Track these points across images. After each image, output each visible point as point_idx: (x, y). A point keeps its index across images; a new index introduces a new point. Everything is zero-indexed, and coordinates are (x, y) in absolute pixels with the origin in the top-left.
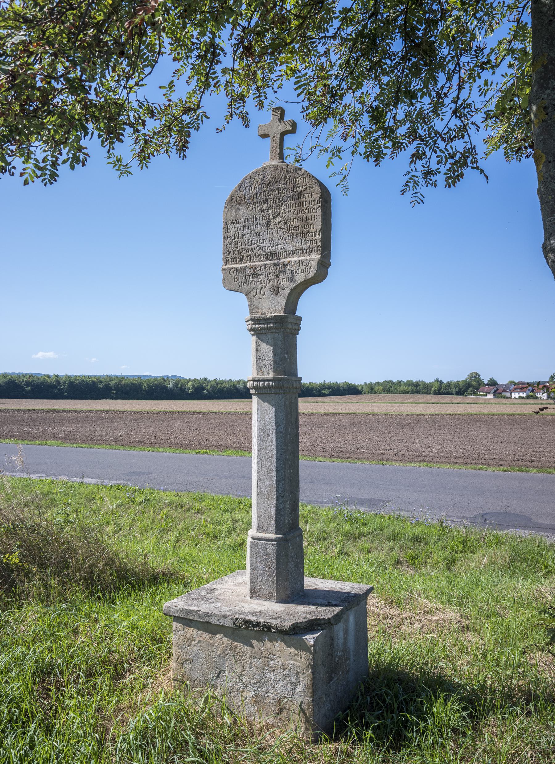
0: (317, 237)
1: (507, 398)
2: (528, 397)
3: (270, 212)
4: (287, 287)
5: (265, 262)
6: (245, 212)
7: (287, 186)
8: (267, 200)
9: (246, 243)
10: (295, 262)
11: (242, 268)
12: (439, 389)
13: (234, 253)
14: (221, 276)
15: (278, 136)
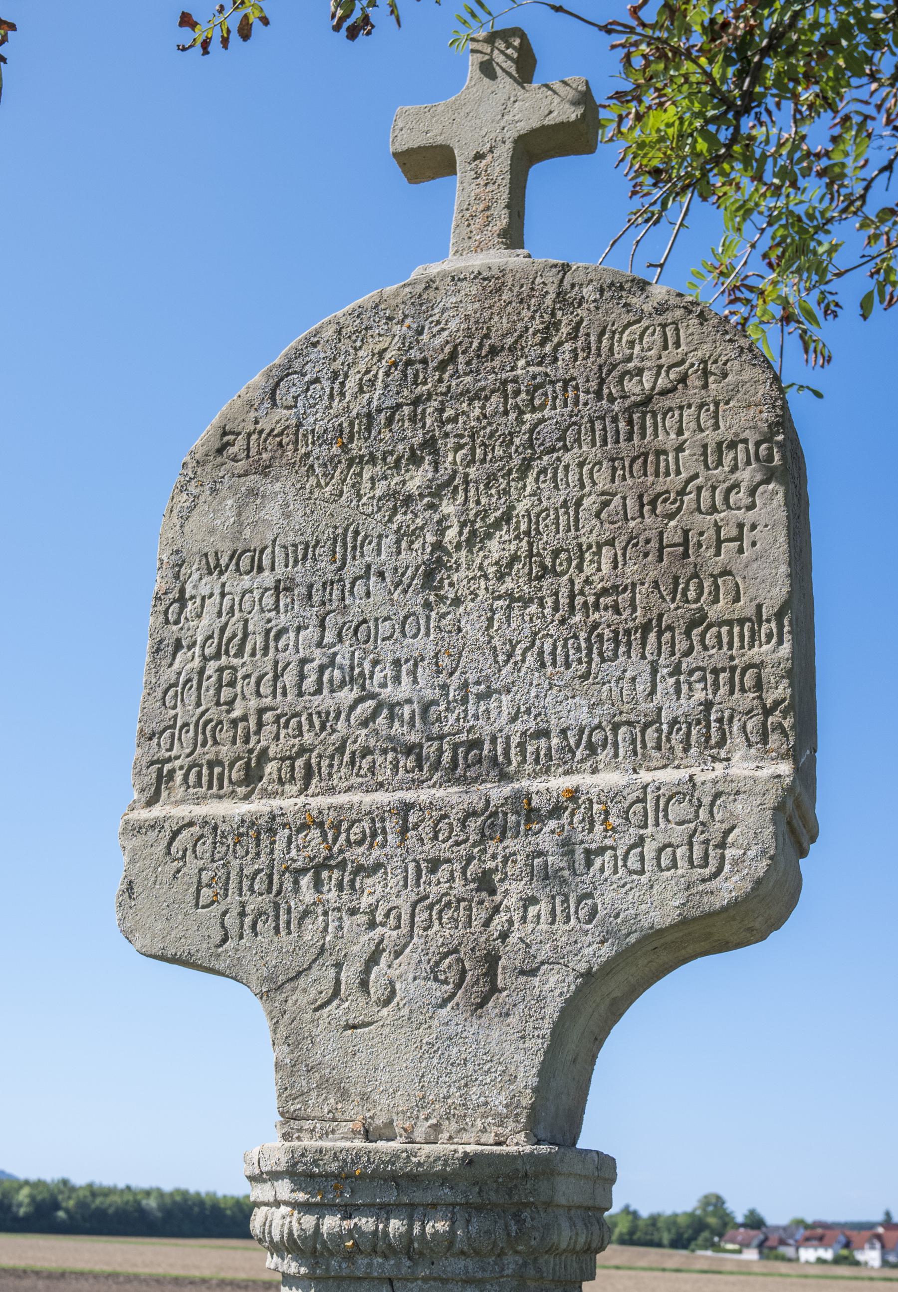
0: (762, 651)
1: (790, 1260)
2: (838, 1260)
3: (448, 508)
4: (558, 948)
5: (409, 796)
6: (298, 510)
7: (560, 370)
8: (430, 444)
9: (289, 678)
10: (616, 795)
11: (252, 823)
12: (632, 1232)
13: (208, 736)
14: (115, 868)
15: (505, 152)
